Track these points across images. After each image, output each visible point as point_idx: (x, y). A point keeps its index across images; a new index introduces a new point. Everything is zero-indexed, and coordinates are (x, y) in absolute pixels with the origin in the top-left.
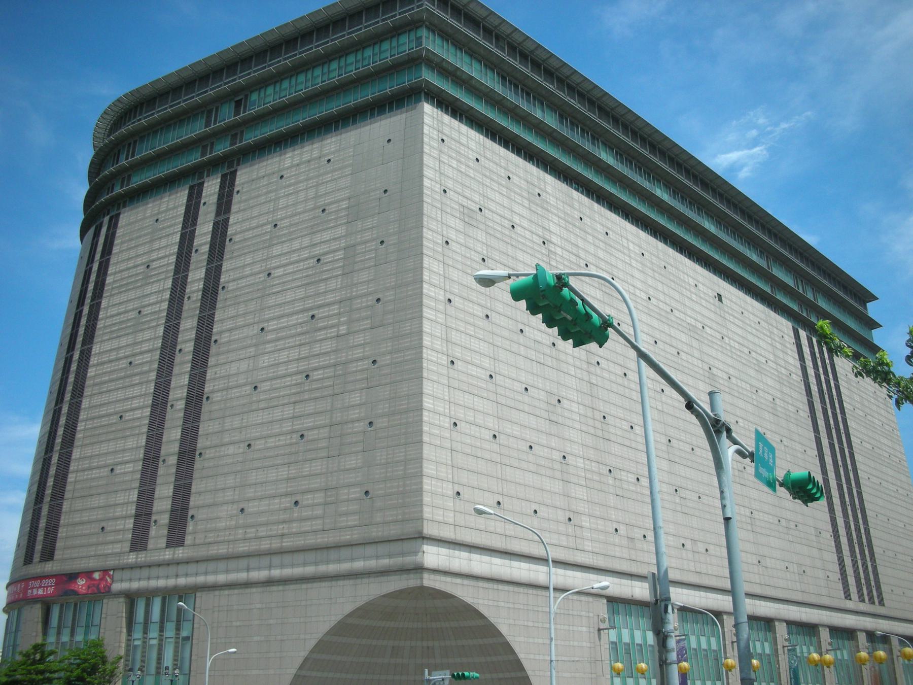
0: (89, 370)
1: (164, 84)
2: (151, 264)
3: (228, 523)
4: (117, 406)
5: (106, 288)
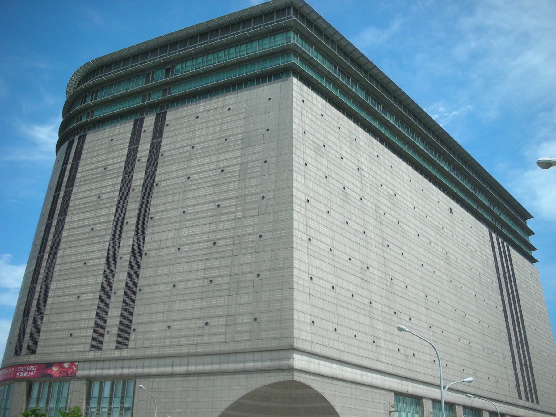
3: (159, 335)
4: (83, 256)
5: (76, 181)
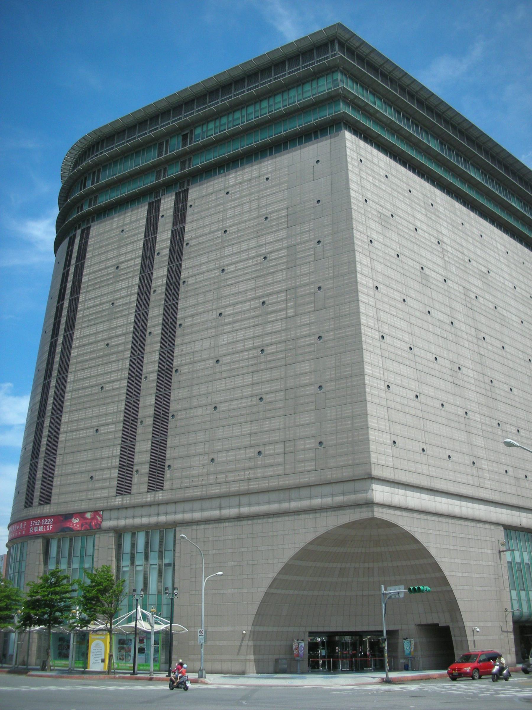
0: (72, 351)
1: (214, 82)
2: (120, 265)
5: (82, 286)
